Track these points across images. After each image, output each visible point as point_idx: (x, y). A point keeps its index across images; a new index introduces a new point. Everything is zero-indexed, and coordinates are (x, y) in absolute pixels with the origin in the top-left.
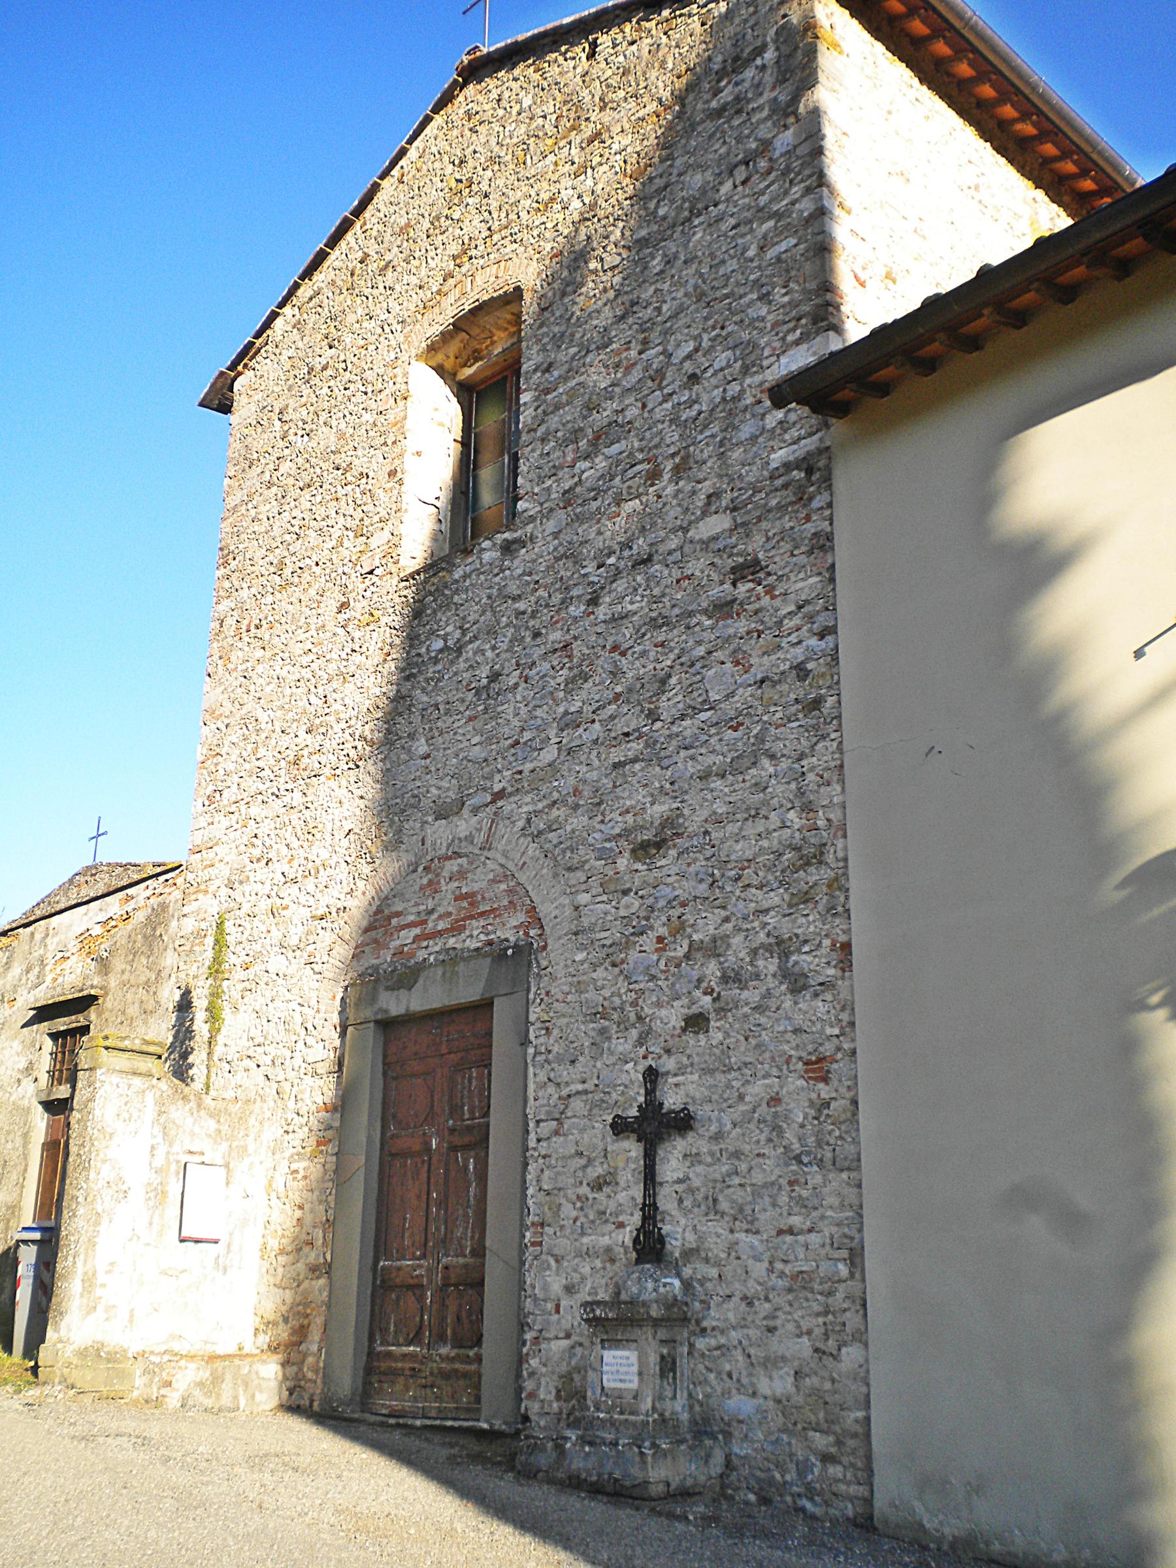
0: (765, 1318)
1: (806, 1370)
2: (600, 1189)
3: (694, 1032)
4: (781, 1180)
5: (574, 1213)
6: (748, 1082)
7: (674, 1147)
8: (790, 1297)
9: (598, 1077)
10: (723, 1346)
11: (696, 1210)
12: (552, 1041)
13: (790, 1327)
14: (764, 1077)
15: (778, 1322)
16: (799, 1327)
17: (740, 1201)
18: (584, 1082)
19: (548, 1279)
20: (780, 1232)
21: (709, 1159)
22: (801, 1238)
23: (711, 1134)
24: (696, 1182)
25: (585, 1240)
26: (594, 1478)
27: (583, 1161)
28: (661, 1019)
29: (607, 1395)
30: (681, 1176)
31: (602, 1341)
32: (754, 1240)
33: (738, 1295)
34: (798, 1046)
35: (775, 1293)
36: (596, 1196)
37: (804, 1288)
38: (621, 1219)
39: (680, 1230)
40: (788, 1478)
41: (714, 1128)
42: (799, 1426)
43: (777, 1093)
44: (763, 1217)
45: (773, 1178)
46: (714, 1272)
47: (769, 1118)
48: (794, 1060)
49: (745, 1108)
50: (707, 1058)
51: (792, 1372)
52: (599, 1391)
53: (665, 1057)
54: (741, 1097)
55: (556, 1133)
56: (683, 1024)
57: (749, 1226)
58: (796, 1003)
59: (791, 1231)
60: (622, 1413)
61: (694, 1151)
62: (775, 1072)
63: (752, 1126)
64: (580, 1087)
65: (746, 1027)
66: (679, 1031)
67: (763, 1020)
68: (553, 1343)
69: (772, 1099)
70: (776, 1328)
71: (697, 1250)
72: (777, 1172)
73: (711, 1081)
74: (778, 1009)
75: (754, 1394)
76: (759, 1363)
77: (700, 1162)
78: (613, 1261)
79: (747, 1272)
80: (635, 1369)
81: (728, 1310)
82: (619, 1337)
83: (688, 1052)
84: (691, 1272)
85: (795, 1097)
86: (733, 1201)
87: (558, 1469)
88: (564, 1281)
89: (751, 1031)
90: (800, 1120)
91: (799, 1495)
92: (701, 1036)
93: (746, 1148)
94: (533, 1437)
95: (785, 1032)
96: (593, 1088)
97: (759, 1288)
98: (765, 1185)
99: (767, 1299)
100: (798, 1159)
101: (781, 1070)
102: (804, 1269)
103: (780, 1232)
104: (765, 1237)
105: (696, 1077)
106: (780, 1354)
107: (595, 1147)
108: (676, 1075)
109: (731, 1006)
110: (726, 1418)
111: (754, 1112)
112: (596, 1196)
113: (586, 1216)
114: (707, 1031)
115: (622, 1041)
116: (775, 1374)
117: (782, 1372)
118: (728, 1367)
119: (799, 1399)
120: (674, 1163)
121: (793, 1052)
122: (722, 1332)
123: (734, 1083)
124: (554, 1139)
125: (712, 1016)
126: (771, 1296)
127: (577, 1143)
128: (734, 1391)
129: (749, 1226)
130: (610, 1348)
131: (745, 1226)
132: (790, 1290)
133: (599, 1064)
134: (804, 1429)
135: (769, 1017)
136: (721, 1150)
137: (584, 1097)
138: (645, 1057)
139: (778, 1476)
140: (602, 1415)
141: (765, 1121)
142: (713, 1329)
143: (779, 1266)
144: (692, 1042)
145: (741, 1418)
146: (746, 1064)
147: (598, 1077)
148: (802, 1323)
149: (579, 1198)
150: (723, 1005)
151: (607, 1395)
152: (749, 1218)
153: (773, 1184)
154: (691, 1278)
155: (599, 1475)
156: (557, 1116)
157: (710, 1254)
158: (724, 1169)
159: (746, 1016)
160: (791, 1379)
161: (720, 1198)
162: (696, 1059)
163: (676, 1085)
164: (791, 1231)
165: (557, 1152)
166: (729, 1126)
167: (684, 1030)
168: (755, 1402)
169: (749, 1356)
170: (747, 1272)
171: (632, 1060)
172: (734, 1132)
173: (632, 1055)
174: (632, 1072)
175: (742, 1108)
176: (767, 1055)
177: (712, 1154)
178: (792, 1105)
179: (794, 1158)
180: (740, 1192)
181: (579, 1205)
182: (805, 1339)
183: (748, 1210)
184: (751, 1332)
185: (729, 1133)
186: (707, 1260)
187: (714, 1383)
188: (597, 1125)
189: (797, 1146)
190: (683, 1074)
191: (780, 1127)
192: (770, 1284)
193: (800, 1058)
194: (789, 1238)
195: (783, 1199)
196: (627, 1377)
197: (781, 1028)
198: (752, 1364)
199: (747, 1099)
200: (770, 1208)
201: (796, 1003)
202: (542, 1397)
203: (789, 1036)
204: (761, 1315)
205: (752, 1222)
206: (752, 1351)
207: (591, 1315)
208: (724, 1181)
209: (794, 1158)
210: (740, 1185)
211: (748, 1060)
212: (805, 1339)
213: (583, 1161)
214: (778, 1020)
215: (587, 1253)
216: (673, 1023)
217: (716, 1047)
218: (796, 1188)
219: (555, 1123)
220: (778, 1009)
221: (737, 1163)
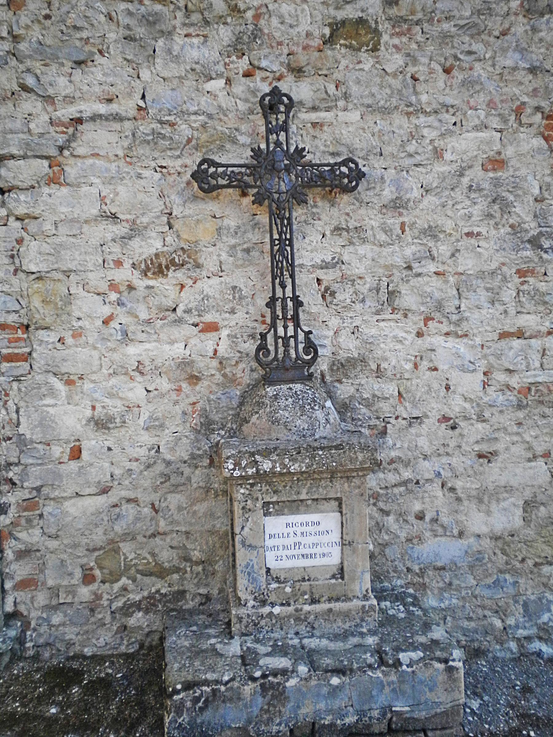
0: (477, 442)
1: (541, 497)
2: (160, 271)
3: (349, 47)
4: (505, 269)
5: (107, 311)
6: (450, 133)
7: (316, 217)
8: (521, 415)
9: (143, 97)
10: (409, 481)
11: (358, 306)
12: (24, 20)
13: (518, 450)
14: (476, 128)
15: (500, 446)
16: (530, 448)
17: (437, 295)
18: (110, 101)
19: (51, 410)
20: (504, 335)
21: (382, 237)
22: (535, 343)
23: (385, 201)
24: (358, 268)
25: (132, 350)
26: (350, 719)
27: (120, 230)
28: (281, 17)
29: (277, 580)
30: (328, 259)
31: (266, 504)
32: (461, 346)
33: (435, 416)
34: (535, 90)
35: (494, 410)
36: (151, 283)
37: (541, 402)
38: (208, 318)
39: (331, 333)
40: (511, 621)
41: (388, 193)
42: (530, 563)
43: (499, 153)
44: (475, 316)
45: (494, 265)
46: (391, 389)
47: (486, 185)
48: (529, 111)
49: (446, 168)
50: (375, 90)
51: (521, 503)
52: (263, 579)
53: (290, 78)
54: (438, 154)
55: (52, 181)
56: (327, 31)
57: (452, 328)
58: (534, 30)
59: (520, 334)
60: (314, 601)
61: (352, 224)
62: (495, 123)
63: (458, 195)
64: (102, 109)
65: (448, 52)
66: (317, 42)
67: (477, 47)
68: (67, 504)
69: (491, 160)
70: (494, 454)
71: (363, 360)
72: (499, 258)
73: (381, 124)
74: (504, 33)
75: (461, 534)
76: (469, 497)
77: (364, 241)
78: (194, 379)
79: (448, 388)
80: (335, 536)
81: (418, 435)
82: (303, 496)
83: (337, 75)
84: (352, 390)
85: (529, 159)
86: (423, 295)
87: (270, 720)
88: (88, 413)
89: (456, 58)
90: (536, 191)
91: (528, 639)
92: (363, 55)
93: (449, 225)
94: (206, 683)
95: (515, 69)
96: (132, 113)
97: (467, 405)
98: (481, 275)
99: (481, 419)
100: (535, 243)
101: (506, 121)
102: (540, 379)
103: (504, 335)
104: (478, 340)
105: (354, 116)
106: (503, 483)
107: (145, 209)
108: (314, 109)
109: (420, 15)
110: (416, 568)
111: (462, 175)
112: (151, 283)
113: (132, 313)
114: (375, 49)
115: (195, 41)
116: (494, 506)
117: (504, 504)
118: (417, 507)
119: (530, 532)
120: (314, 237)
121: (525, 99)
122: (407, 464)
123: (425, 132)
124: (46, 190)
125: (384, 27)
126: (487, 414)
127: (102, 199)
128: (428, 534)
129: (452, 328)
130: (279, 513)
131: (445, 328)
132: (520, 407)
133: (145, 74)
134: (536, 565)
135: (487, 44)
136: (403, 224)
137: (117, 126)
138: (247, 75)
139: (498, 624)
140: (277, 610)
141: (480, 190)
142: (392, 462)
143: (500, 377)
144: (344, 63)
145: (439, 564)
146: (446, 107)
147: (143, 97)
148: (535, 444)
149: (113, 286)
150: (403, 13)
151: (277, 580)
152: (454, 318)
153: (493, 273)
154: (352, 397)
155: (361, 713)
156: (53, 152)
157: (384, 365)
158: (409, 252)
159: (445, 37)
160: (519, 512)
161: (404, 289)
162: (354, 89)
163: (314, 125)
164: (520, 334)
165: (54, 211)
166: (416, 193)
167: (329, 41)
168: (464, 543)
169: (452, 489)
170: (448, 388)
171: (220, 76)
172: (425, 202)
173: (220, 68)
174: (222, 95)
175: (440, 168)
176: (482, 98)
177: (387, 231)
178: (523, 172)
179: (529, 241)
180: (436, 282)
181: (113, 296)
182: (541, 462)
183: (450, 307)
184: (454, 461)
185: (417, 202)
186: (379, 373)
187: (394, 527)
188: (146, 173)
189: (533, 225)
190: (328, 109)
191: (503, 199)
192: (486, 399)
193: (538, 109)
194: (516, 343)
195: (508, 295)
196: (318, 550)
197: (509, 63)
198: (459, 499)
199: (448, 156)
200: (486, 305)
201: (534, 30)
202: (50, 583)
203: (520, 75)
204: (472, 440)
205: (458, 323)
206: (459, 484)
207: (251, 471)
208: (409, 268)
209: (529, 241)
210: (436, 273)
211: (449, 101)
212: (541, 462)
213: (120, 230)
214: (504, 50)
215: (137, 369)
216: (304, 27)
217: (395, 75)
218: (531, 280)
219: (46, 163)
220: (504, 33)
221: (431, 244)
